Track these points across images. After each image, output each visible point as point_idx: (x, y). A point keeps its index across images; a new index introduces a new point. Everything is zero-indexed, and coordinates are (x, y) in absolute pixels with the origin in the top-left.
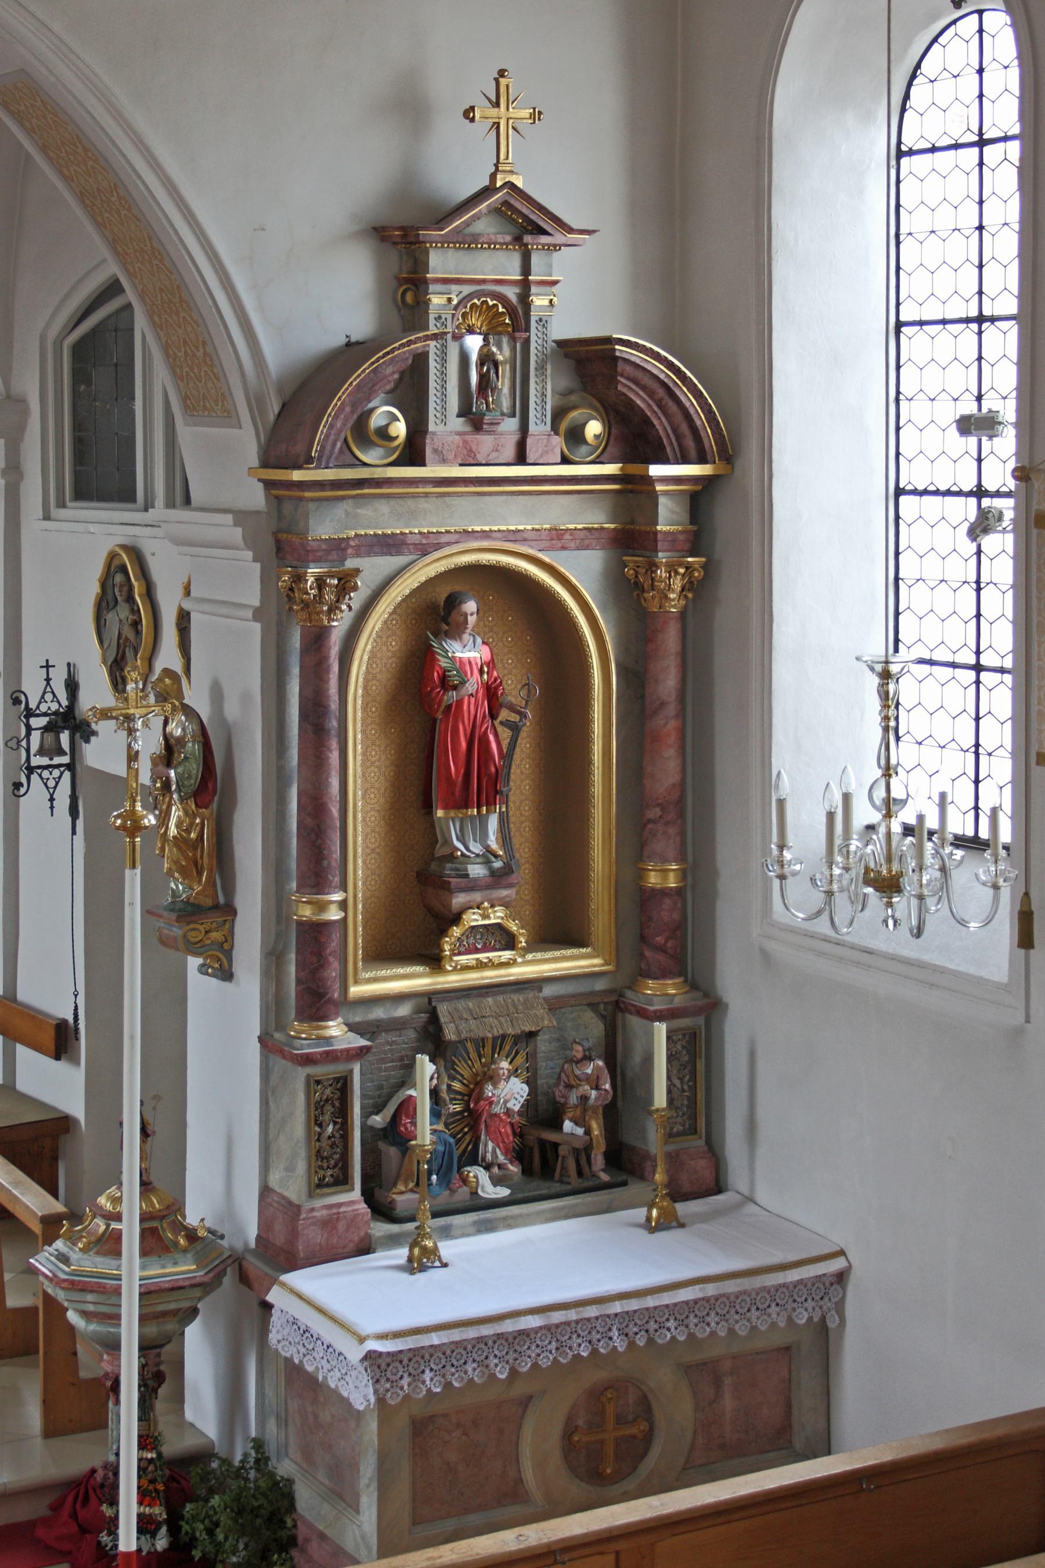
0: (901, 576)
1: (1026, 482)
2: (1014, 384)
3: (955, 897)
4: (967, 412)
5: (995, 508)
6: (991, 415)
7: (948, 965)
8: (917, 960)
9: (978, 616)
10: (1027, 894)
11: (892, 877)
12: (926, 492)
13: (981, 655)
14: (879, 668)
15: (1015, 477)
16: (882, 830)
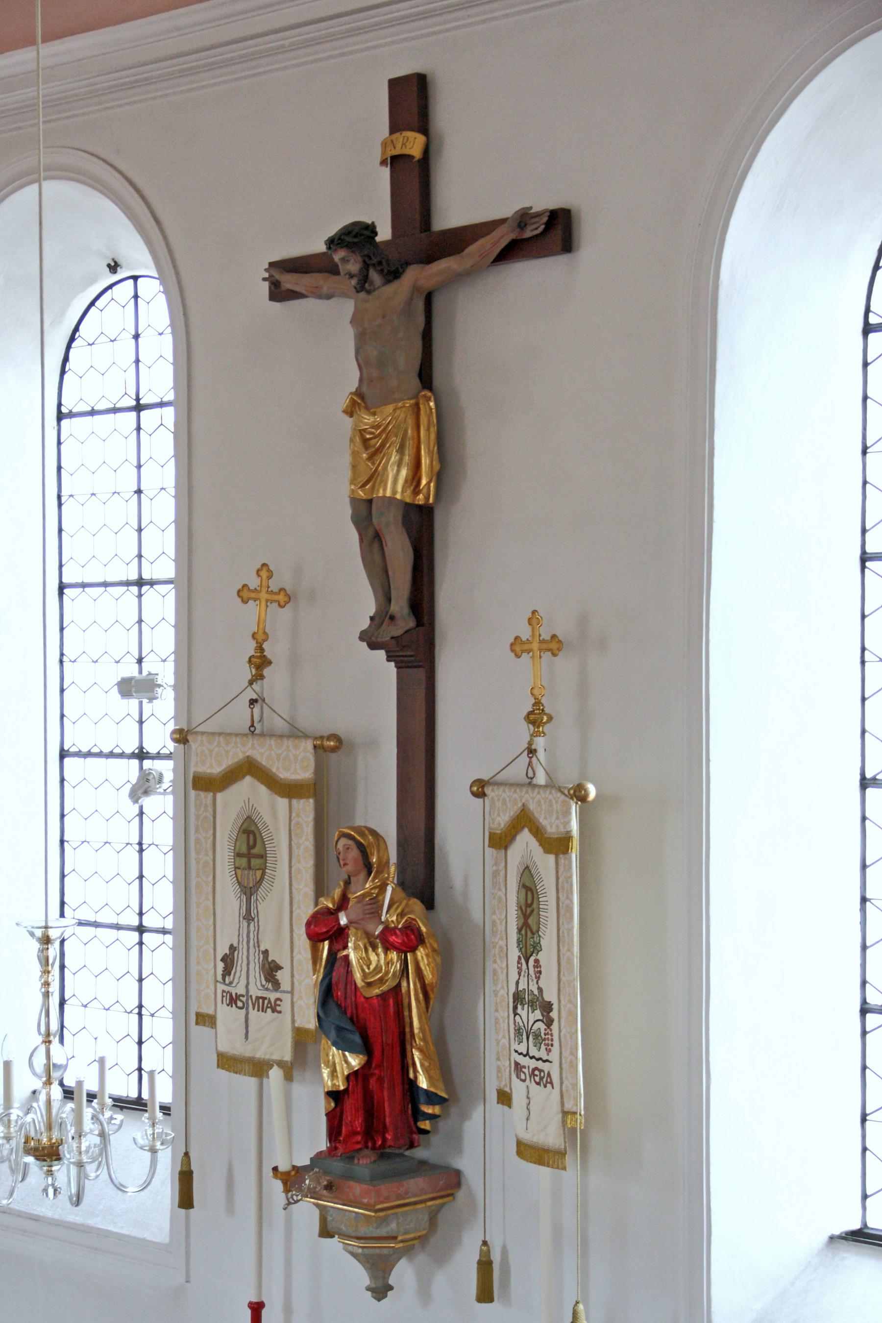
0: (66, 838)
1: (185, 744)
2: (172, 648)
3: (114, 1164)
4: (127, 674)
5: (156, 771)
6: (151, 677)
7: (111, 1228)
8: (82, 1225)
9: (141, 877)
10: (186, 1154)
11: (52, 1145)
12: (89, 754)
13: (144, 917)
14: (39, 933)
15: (175, 740)
16: (42, 1097)
